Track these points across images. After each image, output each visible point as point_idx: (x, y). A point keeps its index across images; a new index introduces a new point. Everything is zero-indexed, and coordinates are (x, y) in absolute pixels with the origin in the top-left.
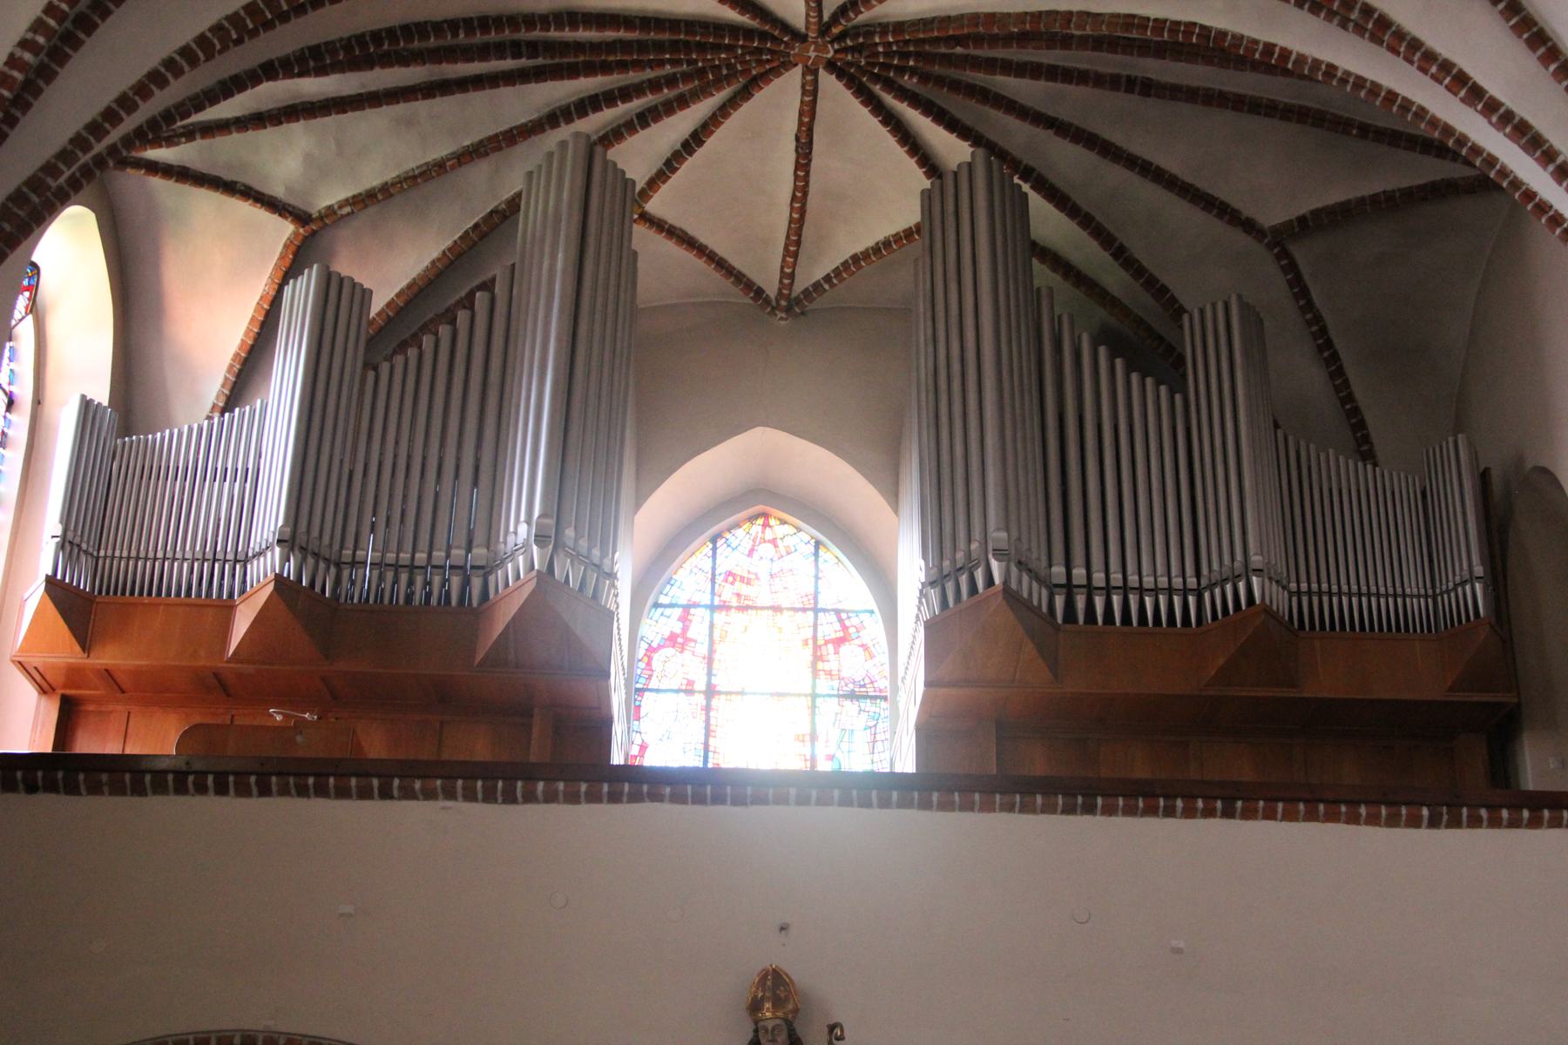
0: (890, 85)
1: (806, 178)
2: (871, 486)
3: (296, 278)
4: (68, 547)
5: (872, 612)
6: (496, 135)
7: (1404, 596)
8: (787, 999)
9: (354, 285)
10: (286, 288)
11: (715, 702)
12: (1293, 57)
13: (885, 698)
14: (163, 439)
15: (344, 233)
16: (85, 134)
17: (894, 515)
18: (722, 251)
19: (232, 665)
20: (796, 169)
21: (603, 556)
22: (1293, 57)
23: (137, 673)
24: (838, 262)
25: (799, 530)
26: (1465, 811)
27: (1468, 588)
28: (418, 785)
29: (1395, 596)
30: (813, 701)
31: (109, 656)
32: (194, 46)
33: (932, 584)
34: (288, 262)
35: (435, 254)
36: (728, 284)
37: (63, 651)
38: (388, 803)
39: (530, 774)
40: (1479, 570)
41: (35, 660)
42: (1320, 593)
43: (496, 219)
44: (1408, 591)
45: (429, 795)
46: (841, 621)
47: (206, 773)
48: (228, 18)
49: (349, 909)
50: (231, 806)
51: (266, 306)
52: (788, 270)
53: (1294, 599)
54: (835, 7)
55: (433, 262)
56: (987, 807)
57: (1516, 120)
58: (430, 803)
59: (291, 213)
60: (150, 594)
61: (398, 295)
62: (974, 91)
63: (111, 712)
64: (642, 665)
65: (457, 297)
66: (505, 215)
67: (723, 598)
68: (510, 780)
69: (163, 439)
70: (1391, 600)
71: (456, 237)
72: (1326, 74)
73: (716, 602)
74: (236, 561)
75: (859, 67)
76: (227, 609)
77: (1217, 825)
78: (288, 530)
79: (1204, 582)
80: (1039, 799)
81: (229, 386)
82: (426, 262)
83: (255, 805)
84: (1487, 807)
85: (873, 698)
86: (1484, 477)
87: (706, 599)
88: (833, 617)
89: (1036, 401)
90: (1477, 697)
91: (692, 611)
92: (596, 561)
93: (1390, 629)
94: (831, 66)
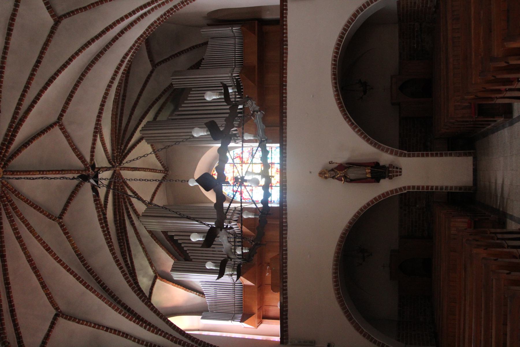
0: (123, 151)
2: (207, 153)
5: (234, 151)
7: (235, 43)
8: (325, 172)
10: (175, 279)
13: (253, 148)
14: (208, 302)
15: (158, 268)
17: (213, 148)
19: (257, 283)
20: (139, 171)
21: (232, 210)
23: (258, 305)
26: (284, 39)
27: (234, 31)
28: (284, 244)
31: (255, 309)
32: (139, 296)
34: (165, 280)
35: (161, 249)
37: (254, 319)
38: (288, 250)
39: (282, 223)
40: (230, 28)
41: (257, 325)
44: (234, 42)
45: (286, 242)
46: (236, 158)
47: (283, 285)
51: (174, 284)
52: (159, 171)
53: (237, 66)
54: (109, 164)
55: (163, 249)
57: (148, 28)
59: (155, 280)
61: (170, 256)
62: (124, 134)
63: (265, 310)
64: (247, 201)
65: (169, 244)
66: (152, 234)
69: (208, 302)
70: (236, 46)
72: (129, 62)
74: (234, 285)
75: (120, 158)
79: (233, 85)
81: (191, 291)
82: (163, 251)
83: (289, 276)
84: (283, 35)
85: (252, 151)
86: (209, 25)
88: (235, 160)
89: (195, 120)
90: (256, 29)
91: (234, 190)
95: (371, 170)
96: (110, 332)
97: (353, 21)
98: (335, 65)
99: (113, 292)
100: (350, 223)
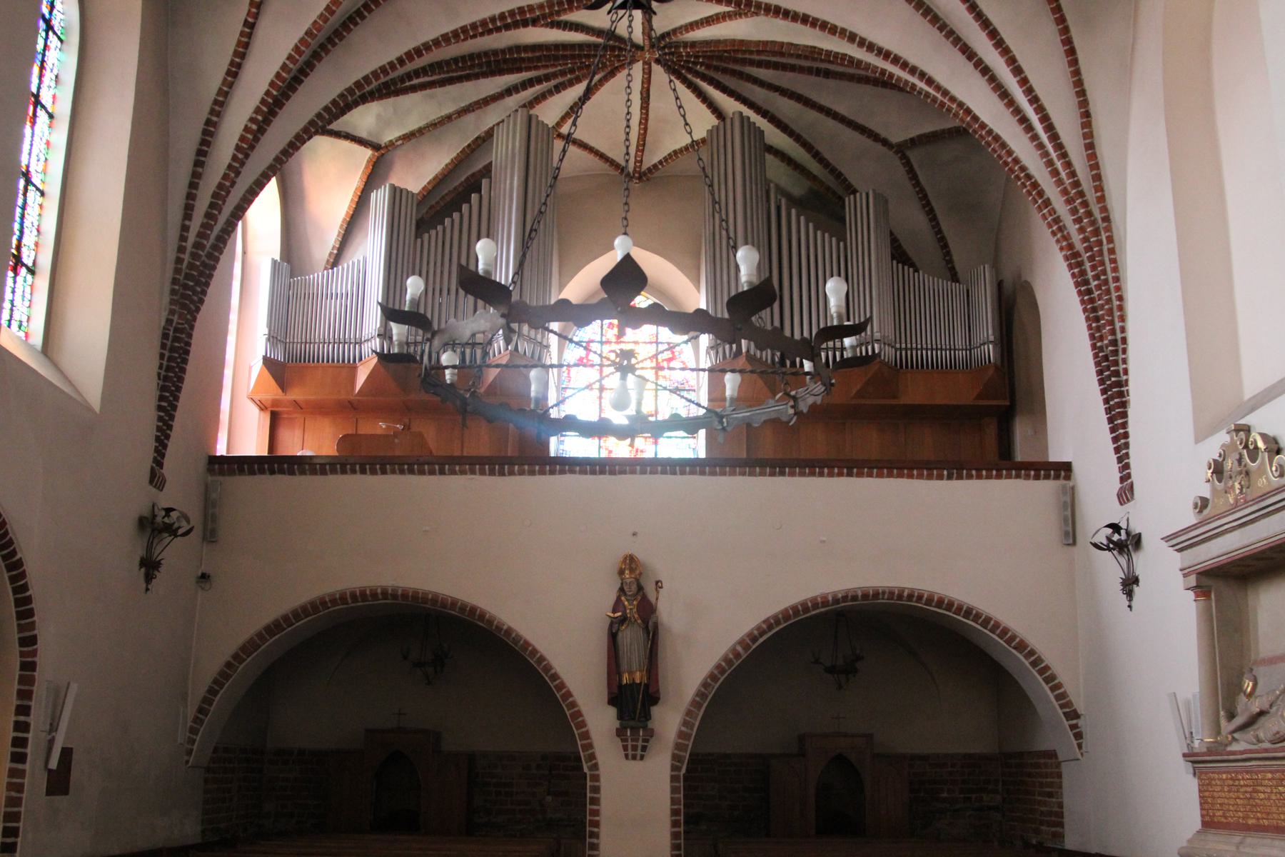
0: (690, 70)
1: (647, 114)
3: (377, 188)
4: (271, 339)
6: (479, 101)
9: (408, 191)
10: (373, 195)
11: (604, 395)
12: (895, 77)
13: (694, 391)
14: (314, 278)
15: (399, 152)
16: (280, 156)
18: (603, 149)
22: (895, 77)
24: (665, 154)
25: (648, 298)
27: (986, 346)
28: (457, 468)
29: (950, 350)
30: (656, 393)
31: (296, 394)
33: (712, 348)
36: (606, 166)
37: (272, 391)
40: (992, 338)
41: (257, 398)
42: (912, 349)
43: (480, 142)
44: (957, 347)
45: (463, 472)
47: (355, 464)
48: (346, 90)
49: (427, 528)
50: (369, 479)
51: (359, 194)
52: (638, 159)
55: (446, 165)
56: (733, 474)
58: (464, 476)
59: (370, 145)
60: (313, 361)
61: (429, 183)
62: (734, 73)
67: (608, 337)
68: (502, 465)
69: (314, 278)
71: (458, 151)
73: (604, 339)
74: (356, 343)
75: (673, 62)
76: (353, 369)
77: (844, 480)
78: (382, 329)
80: (758, 469)
82: (443, 165)
84: (976, 469)
86: (1000, 285)
87: (598, 339)
91: (591, 344)
92: (539, 340)
93: (947, 368)
94: (658, 61)
95: (641, 683)
96: (242, 34)
97: (1009, 642)
98: (900, 597)
99: (341, 40)
100: (509, 631)
